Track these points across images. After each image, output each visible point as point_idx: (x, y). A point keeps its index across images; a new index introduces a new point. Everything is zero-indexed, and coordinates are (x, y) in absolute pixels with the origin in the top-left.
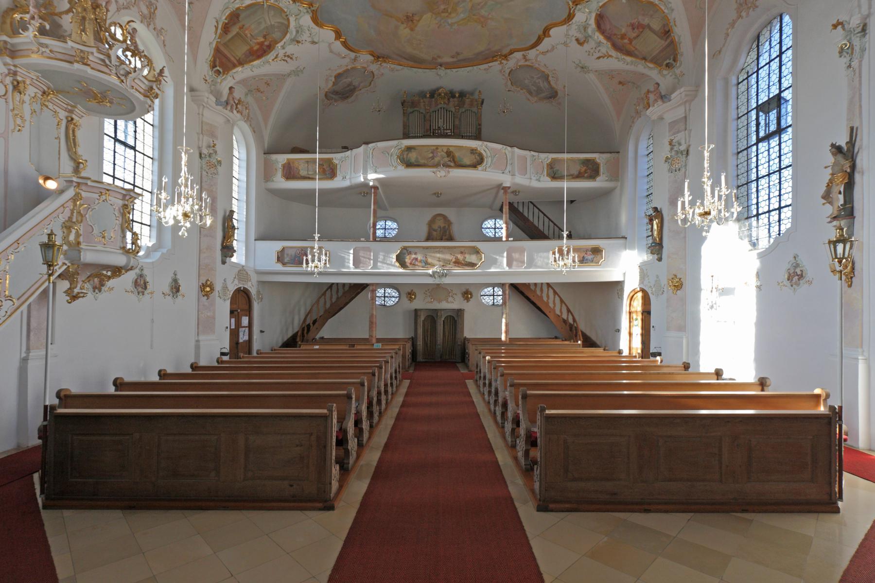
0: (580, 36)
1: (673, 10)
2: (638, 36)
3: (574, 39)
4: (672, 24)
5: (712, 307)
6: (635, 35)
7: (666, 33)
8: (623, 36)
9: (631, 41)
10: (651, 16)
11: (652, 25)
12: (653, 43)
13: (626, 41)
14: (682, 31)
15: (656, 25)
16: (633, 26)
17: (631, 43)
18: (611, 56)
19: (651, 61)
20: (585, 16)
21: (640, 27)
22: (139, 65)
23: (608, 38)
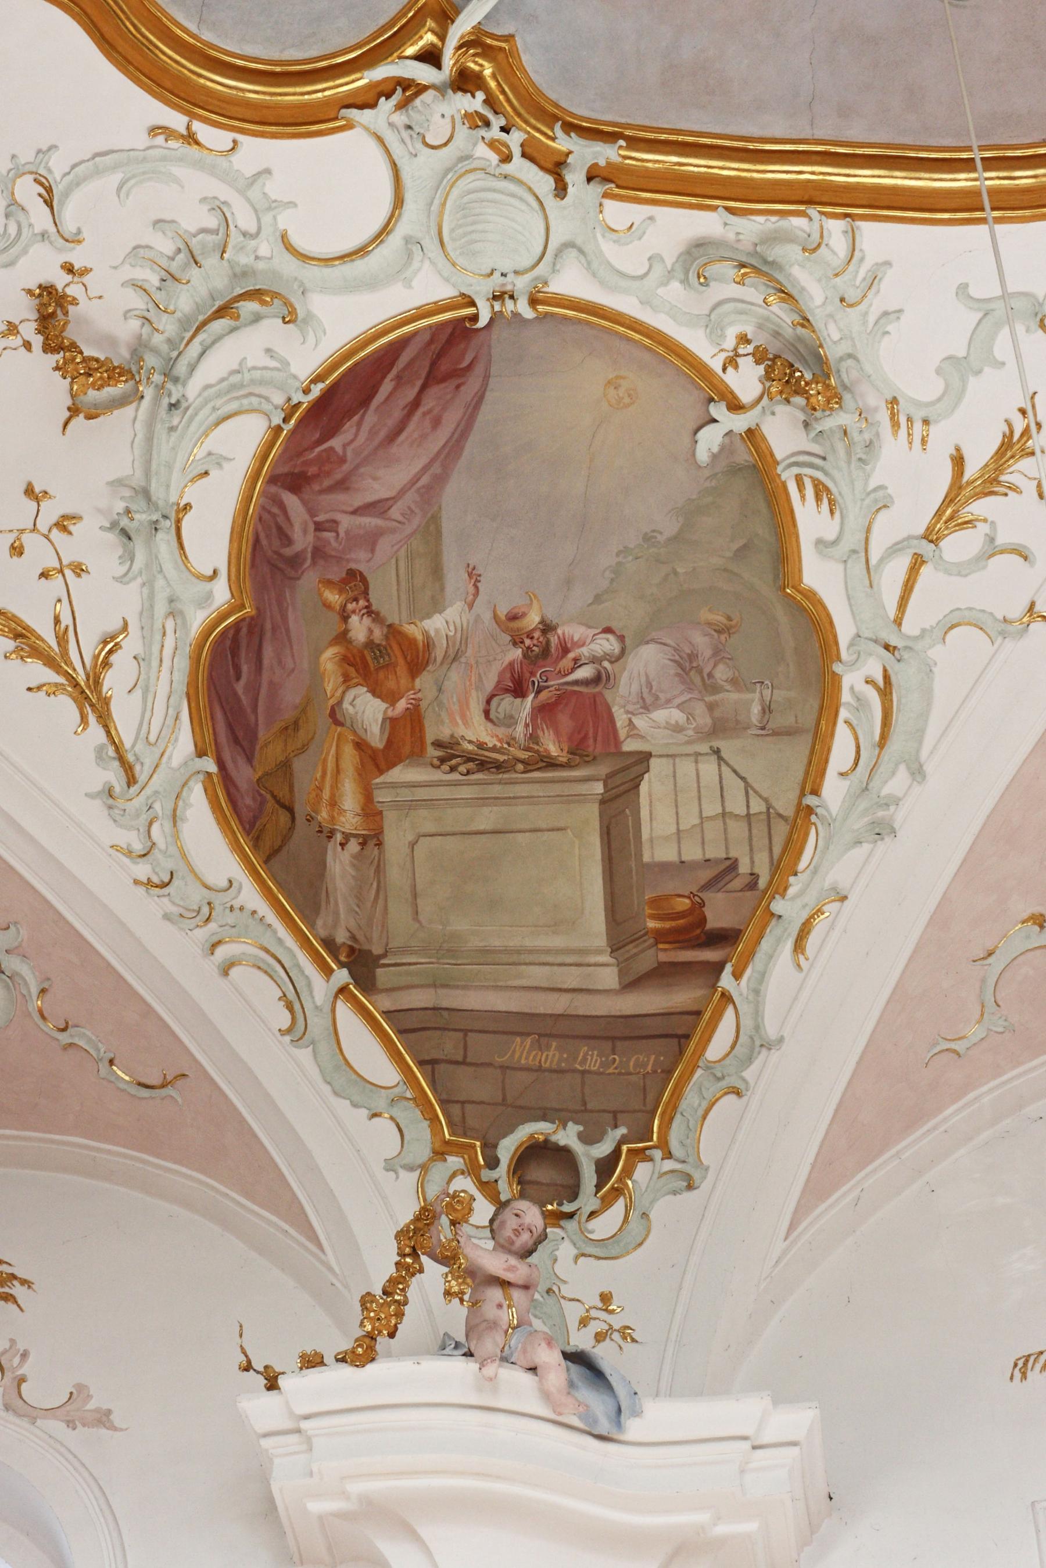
0: (106, 316)
1: (882, 830)
2: (483, 763)
3: (43, 266)
4: (789, 908)
5: (831, 1498)
6: (476, 732)
7: (694, 936)
8: (389, 659)
9: (405, 738)
10: (722, 727)
11: (652, 786)
12: (540, 916)
13: (368, 711)
14: (810, 1006)
15: (674, 818)
16: (534, 662)
17: (376, 760)
18: (90, 698)
19: (414, 1033)
20: (361, 223)
21: (566, 715)
22: (808, 376)
23: (267, 553)
